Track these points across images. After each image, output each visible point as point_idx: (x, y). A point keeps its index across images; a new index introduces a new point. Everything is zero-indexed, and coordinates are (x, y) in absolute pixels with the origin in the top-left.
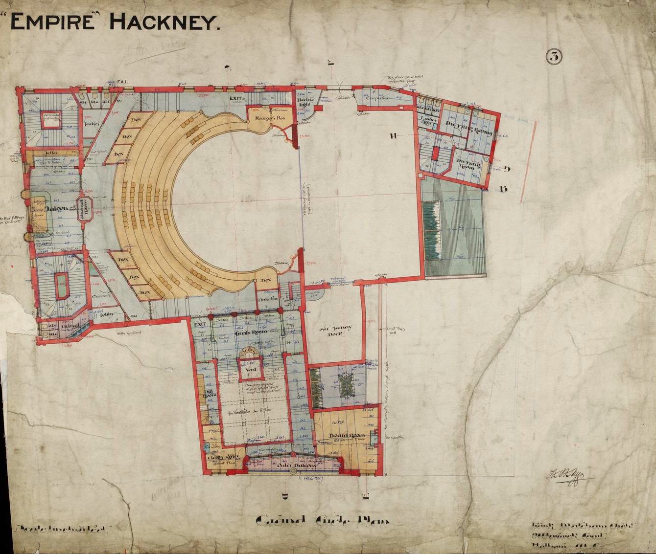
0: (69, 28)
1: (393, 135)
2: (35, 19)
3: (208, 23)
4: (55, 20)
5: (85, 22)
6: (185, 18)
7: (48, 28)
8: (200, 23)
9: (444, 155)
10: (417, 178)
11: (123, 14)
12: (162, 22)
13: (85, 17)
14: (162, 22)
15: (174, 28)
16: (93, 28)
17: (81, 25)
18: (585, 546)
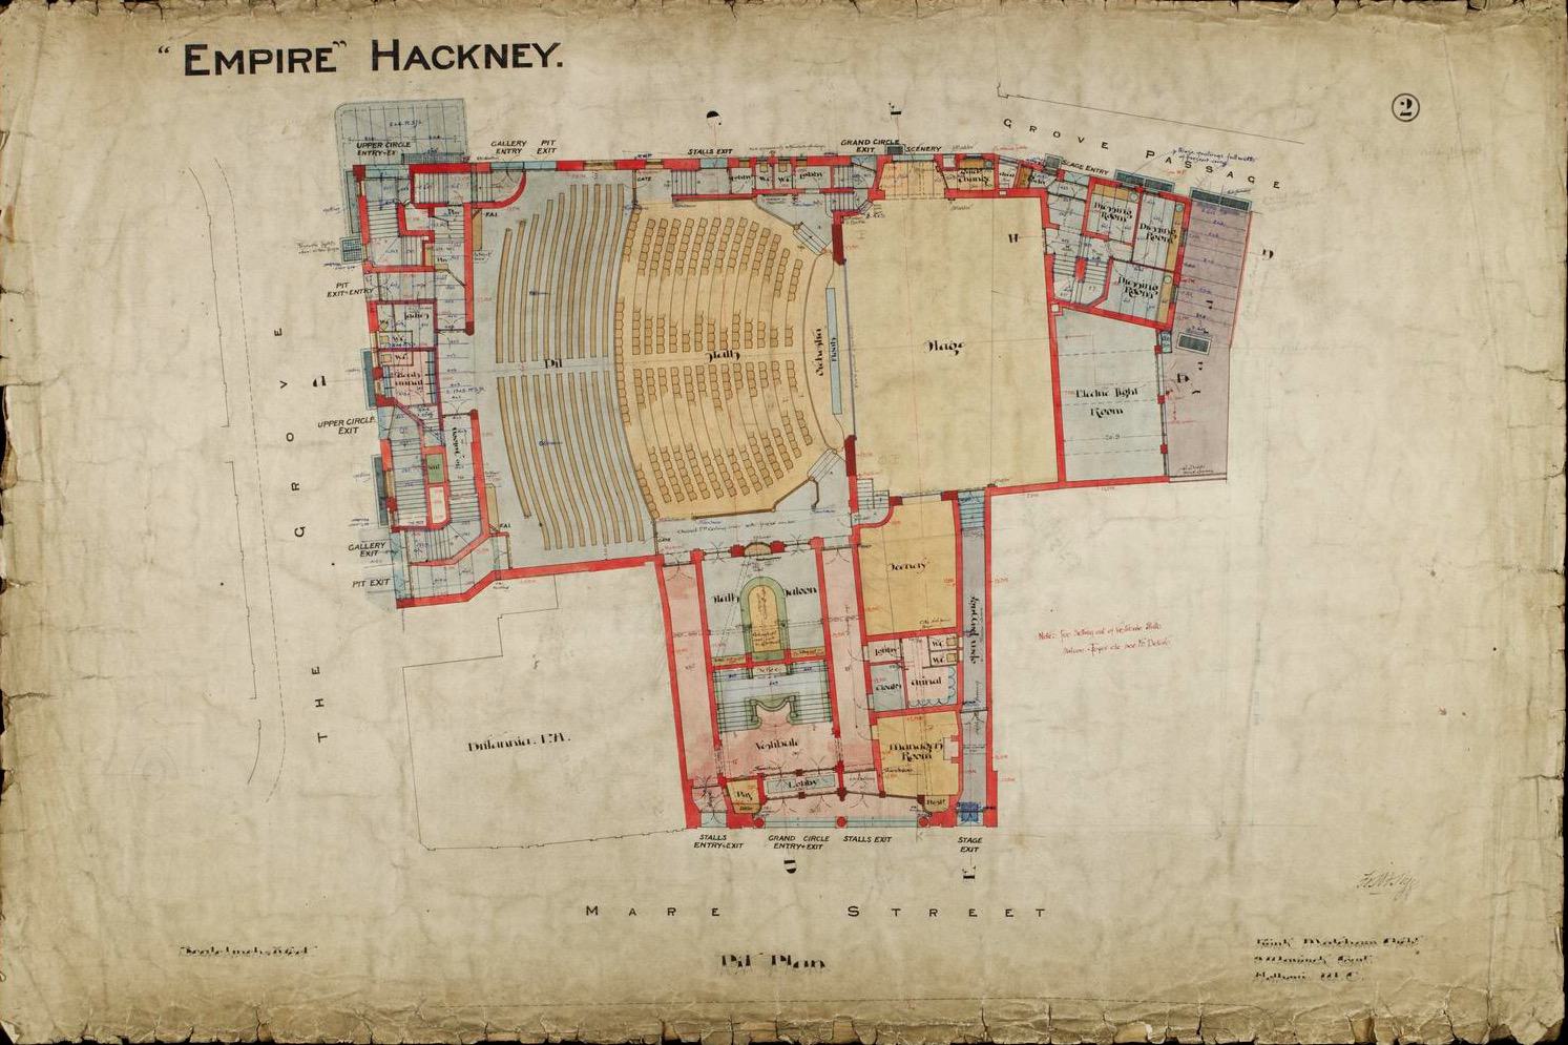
0: (291, 70)
1: (1013, 237)
2: (229, 59)
3: (544, 56)
4: (264, 57)
5: (320, 59)
6: (504, 47)
7: (253, 71)
8: (531, 56)
9: (1096, 273)
10: (1049, 311)
11: (396, 43)
12: (464, 56)
13: (319, 51)
14: (464, 56)
15: (488, 65)
16: (333, 69)
17: (312, 64)
18: (1336, 975)
